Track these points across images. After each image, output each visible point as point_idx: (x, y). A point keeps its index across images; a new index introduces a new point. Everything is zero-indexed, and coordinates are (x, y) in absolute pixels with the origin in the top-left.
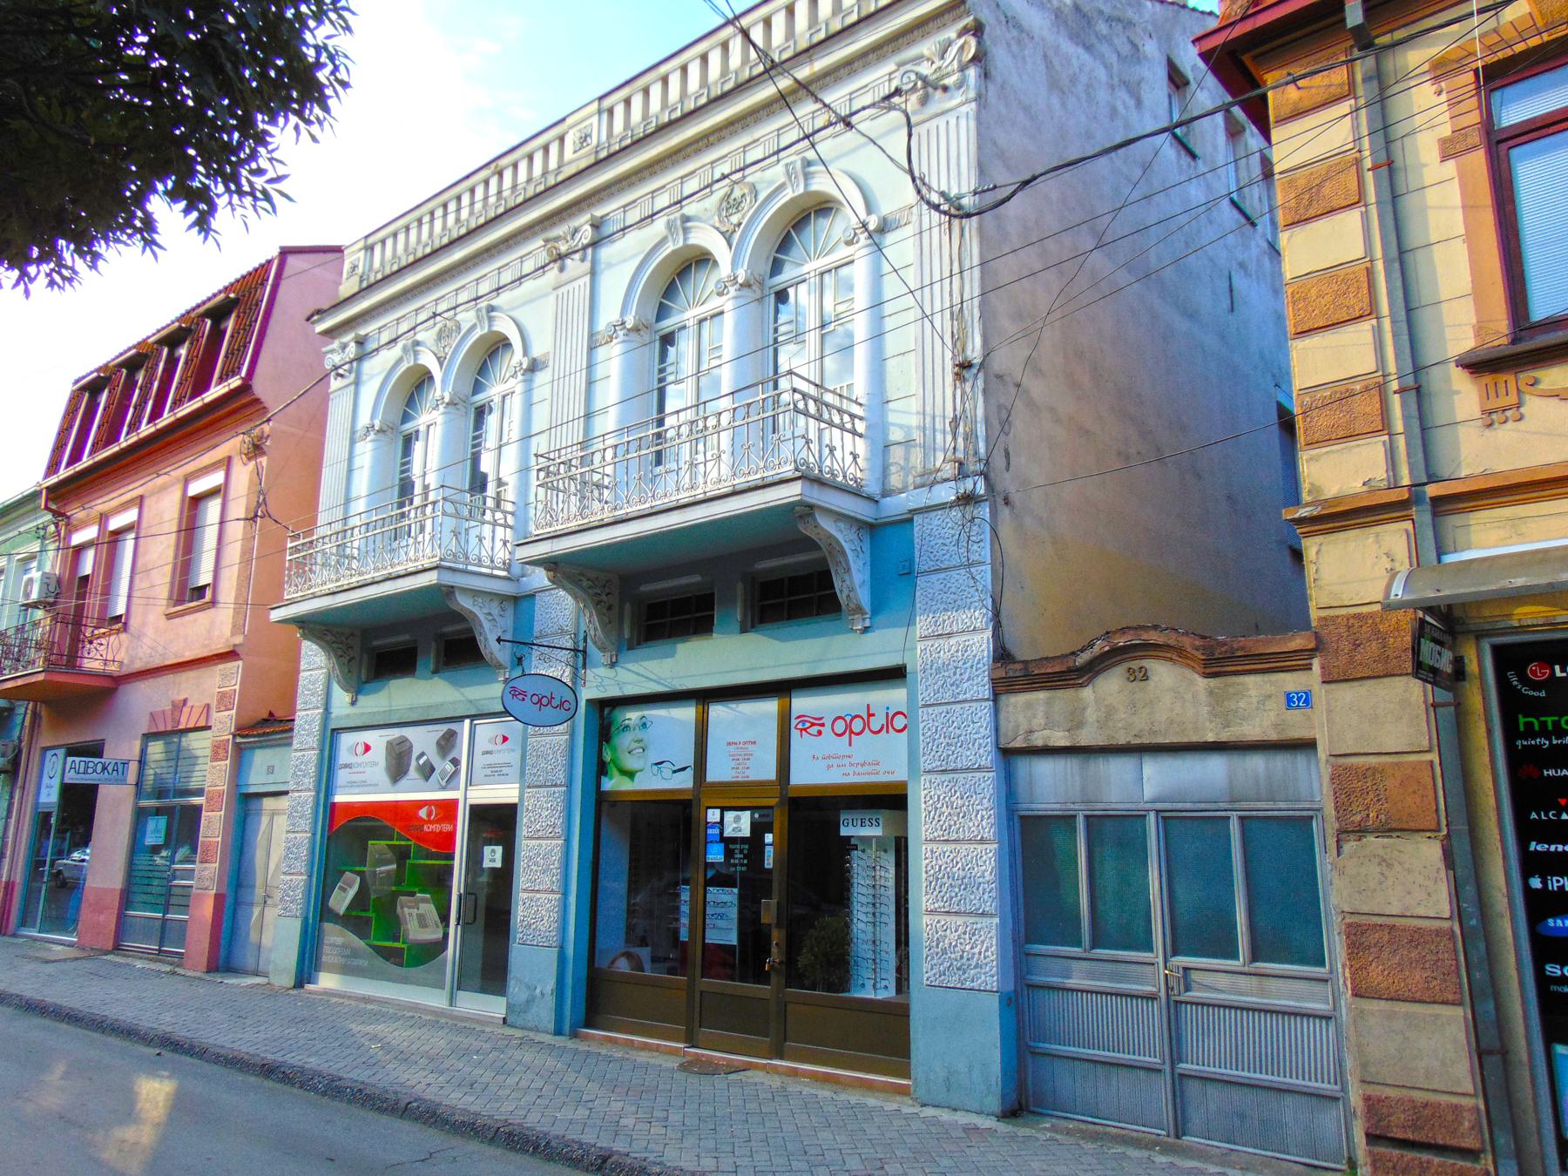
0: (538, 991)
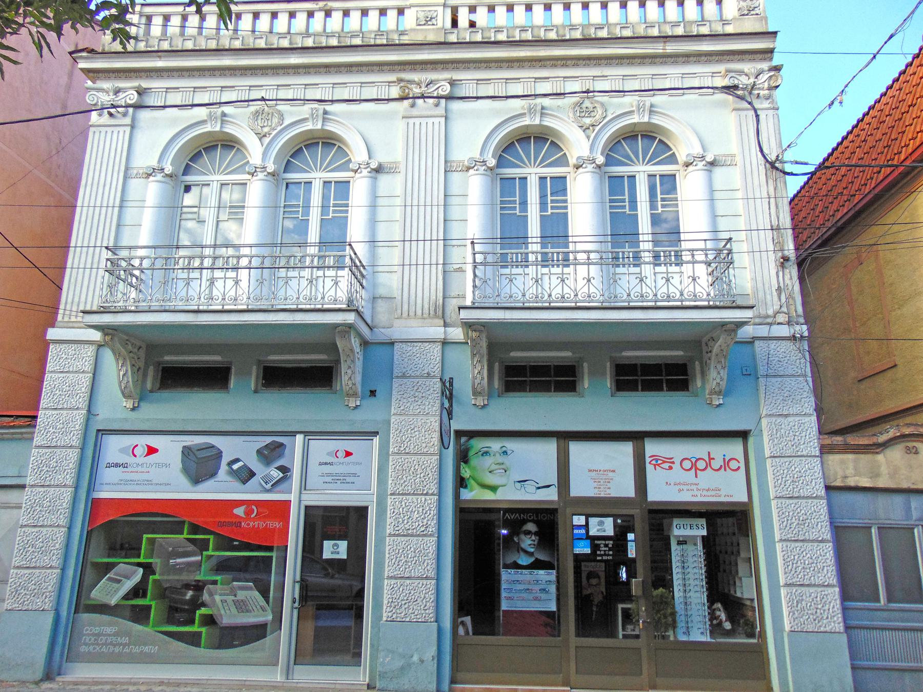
0: (415, 658)
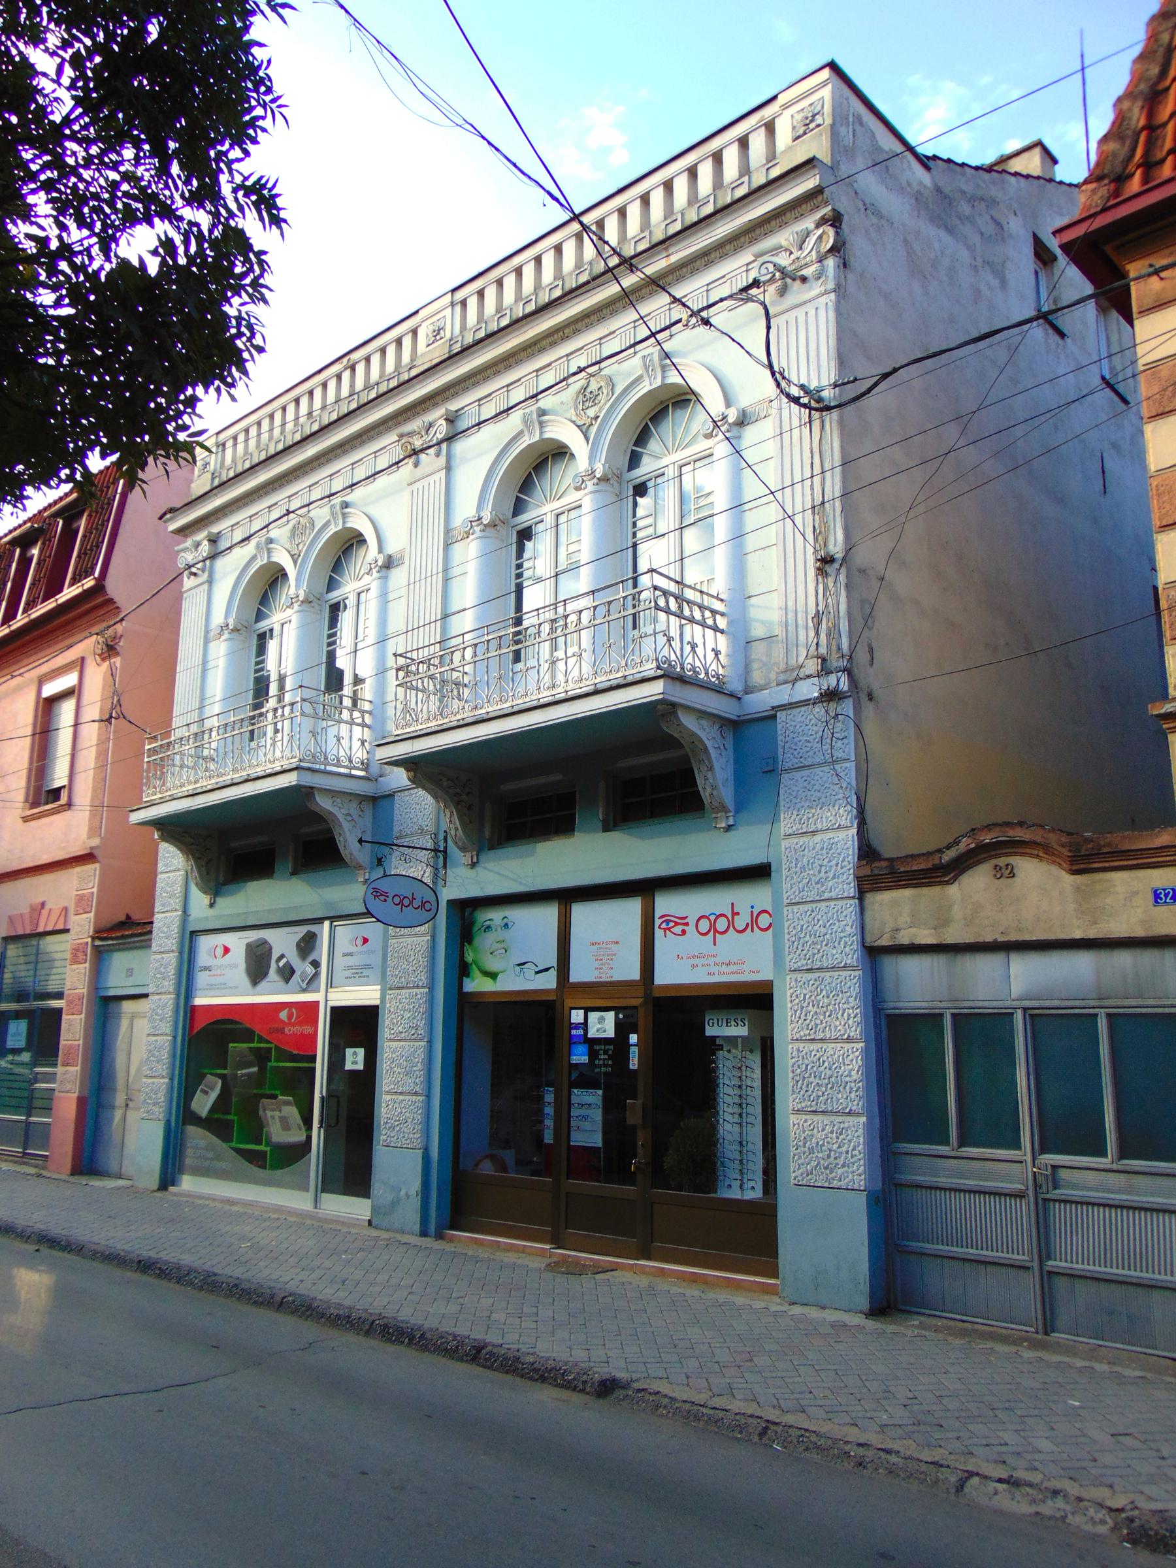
0: (403, 1193)
